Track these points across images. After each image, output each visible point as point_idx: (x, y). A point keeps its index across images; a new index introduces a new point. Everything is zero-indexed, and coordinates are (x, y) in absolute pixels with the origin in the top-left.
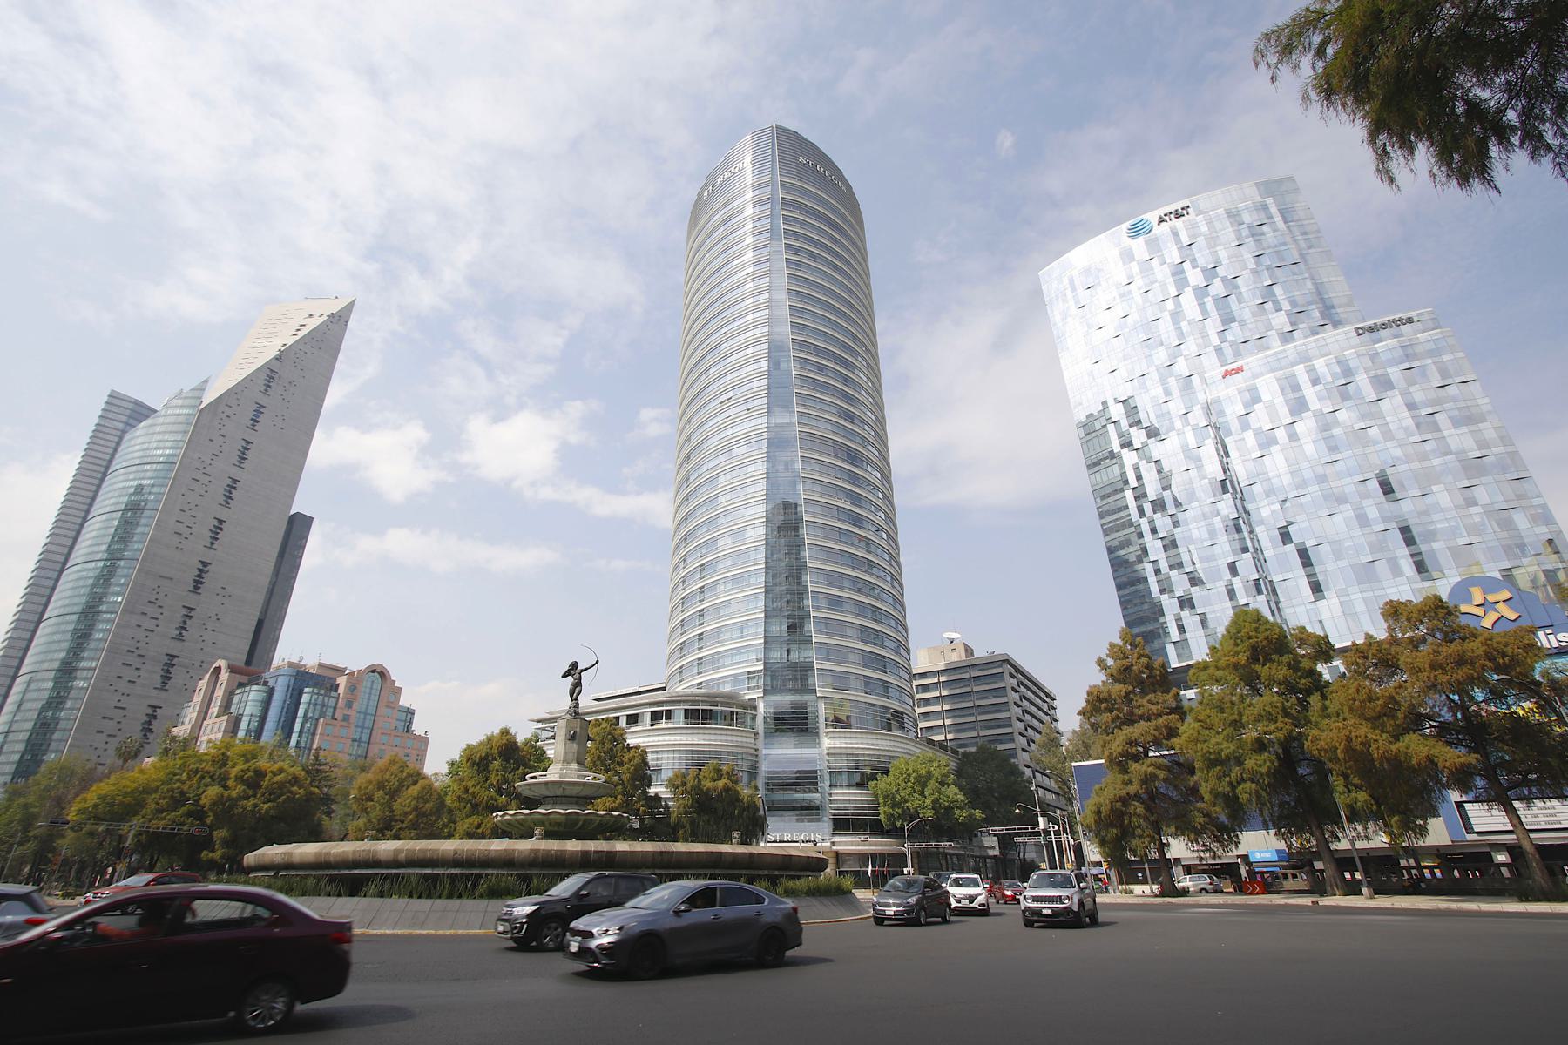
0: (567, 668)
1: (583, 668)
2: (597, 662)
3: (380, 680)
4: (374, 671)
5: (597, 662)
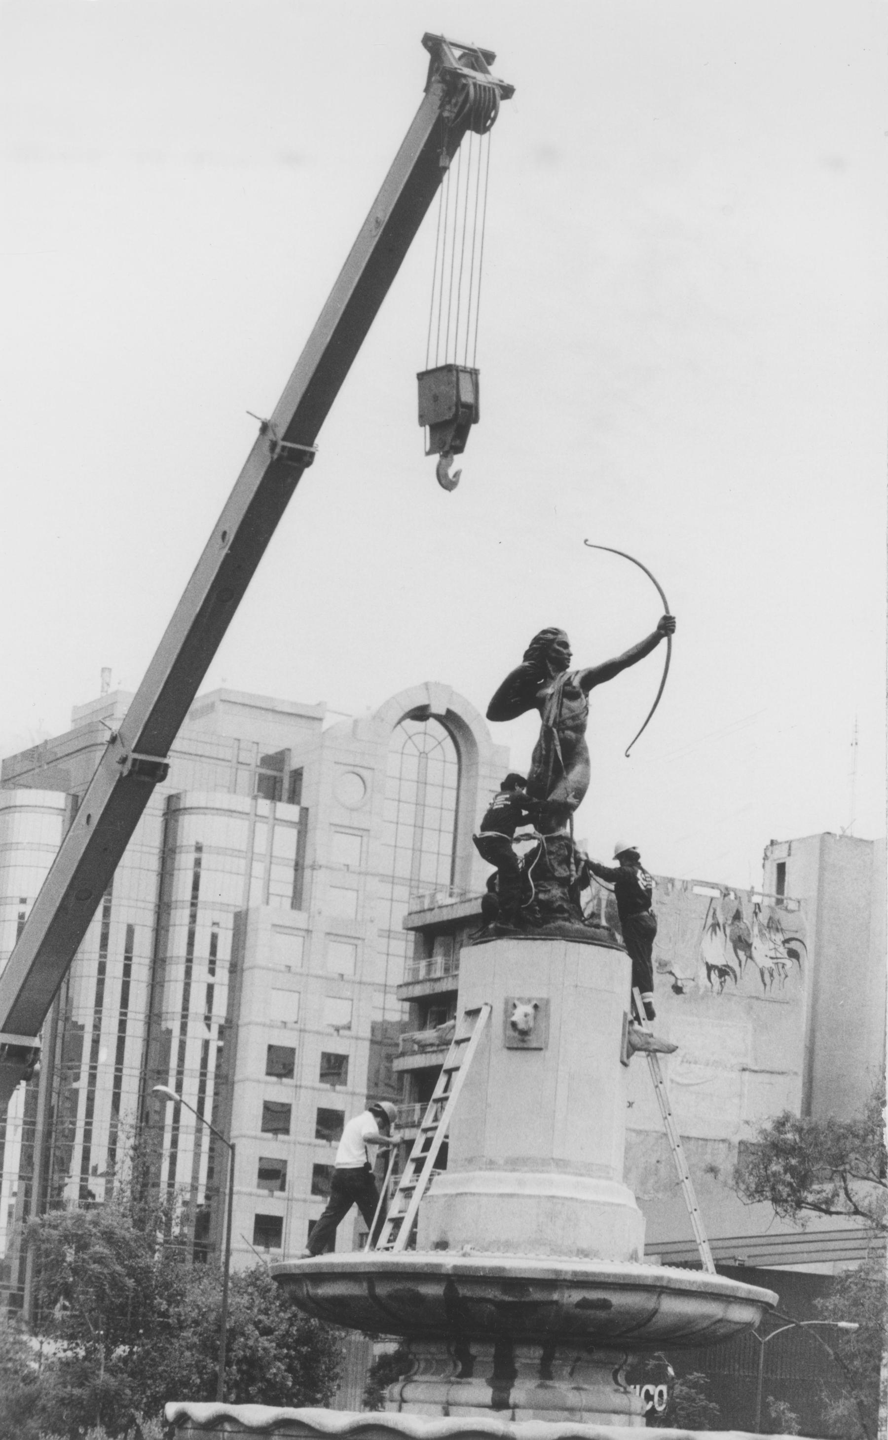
0: (516, 661)
1: (596, 661)
2: (667, 626)
3: (449, 743)
4: (420, 714)
5: (667, 626)
